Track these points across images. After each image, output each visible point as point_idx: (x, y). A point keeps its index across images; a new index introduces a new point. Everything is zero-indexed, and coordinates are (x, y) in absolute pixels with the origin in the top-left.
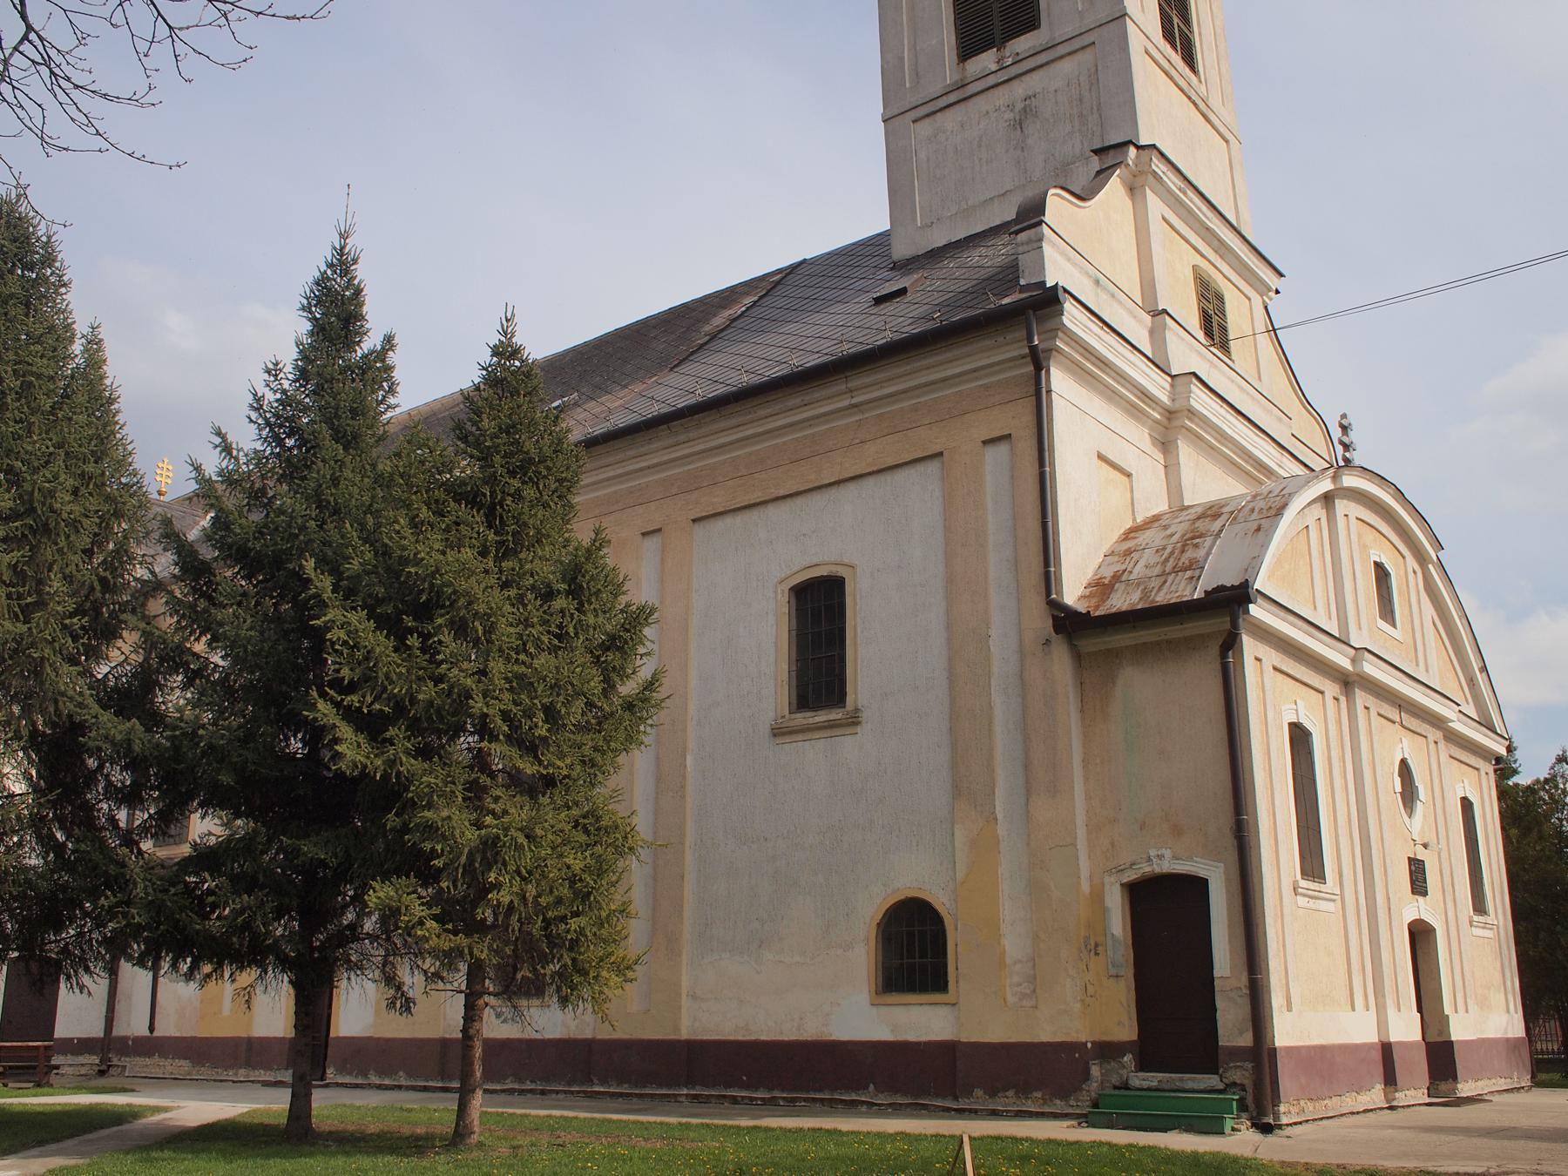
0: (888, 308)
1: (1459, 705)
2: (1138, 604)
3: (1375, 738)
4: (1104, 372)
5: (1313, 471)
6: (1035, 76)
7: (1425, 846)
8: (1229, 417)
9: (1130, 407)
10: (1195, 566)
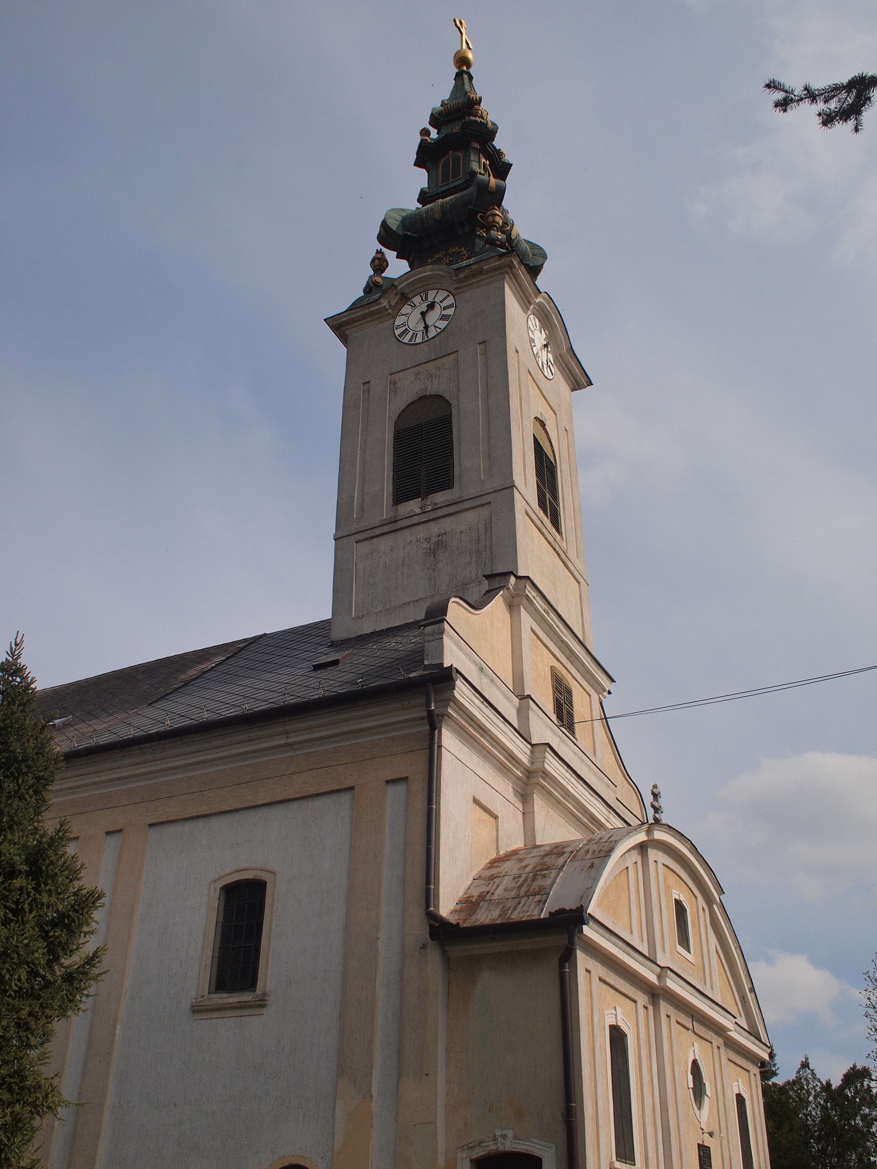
0: (324, 673)
1: (735, 1018)
2: (497, 919)
3: (675, 1042)
4: (482, 736)
5: (630, 825)
6: (448, 520)
7: (711, 1134)
8: (572, 780)
9: (500, 765)
10: (543, 892)
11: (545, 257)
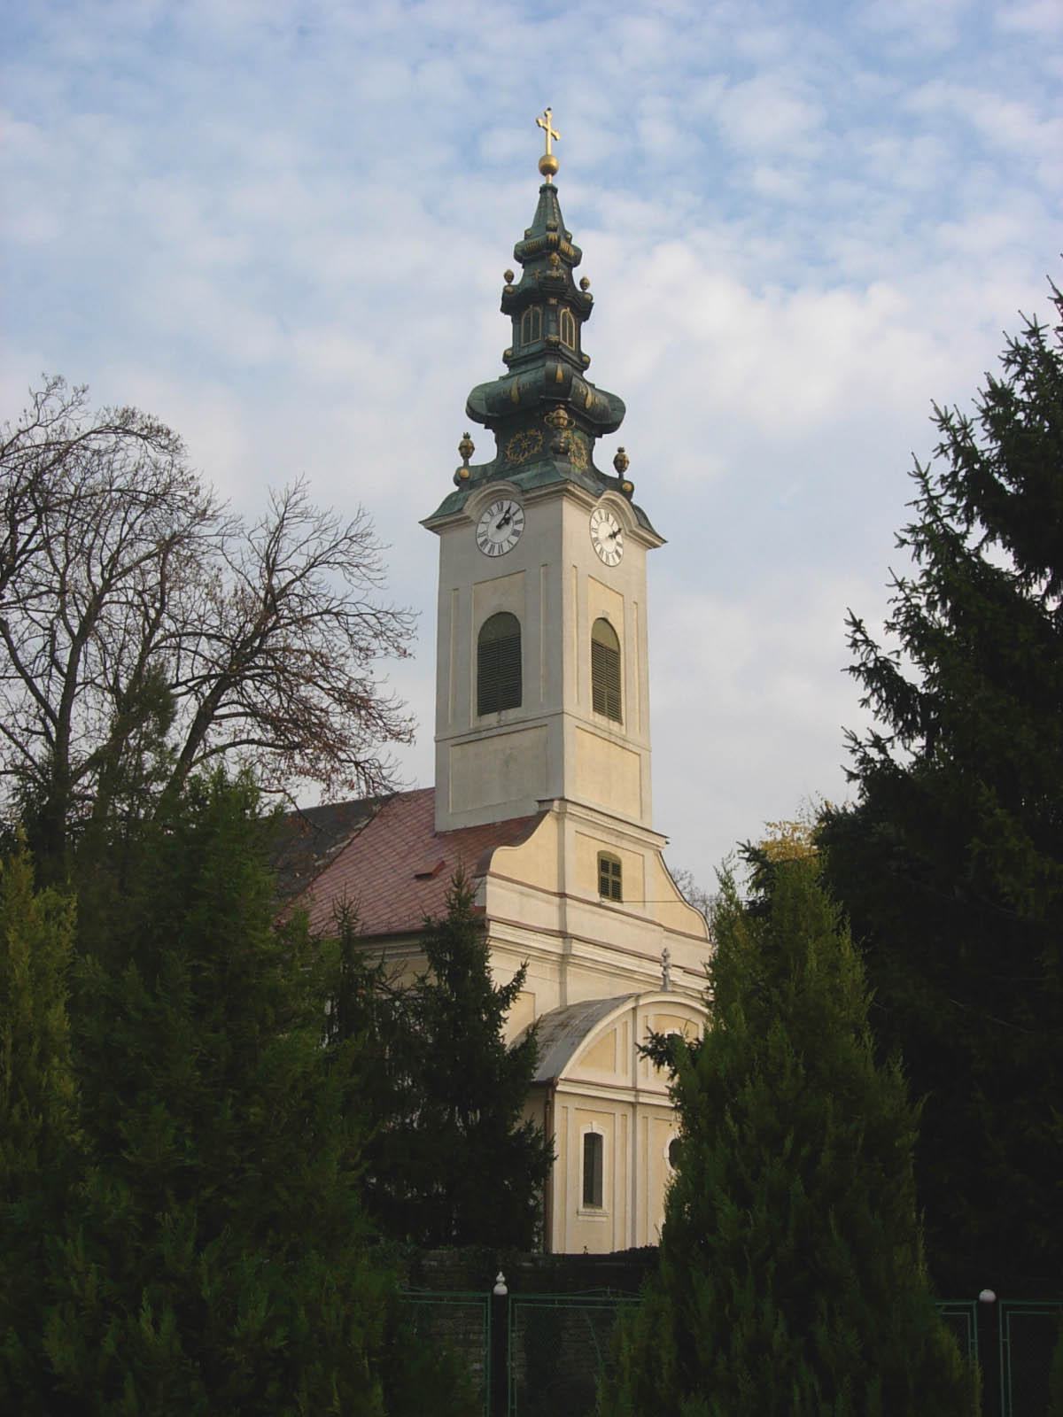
11: (623, 410)
